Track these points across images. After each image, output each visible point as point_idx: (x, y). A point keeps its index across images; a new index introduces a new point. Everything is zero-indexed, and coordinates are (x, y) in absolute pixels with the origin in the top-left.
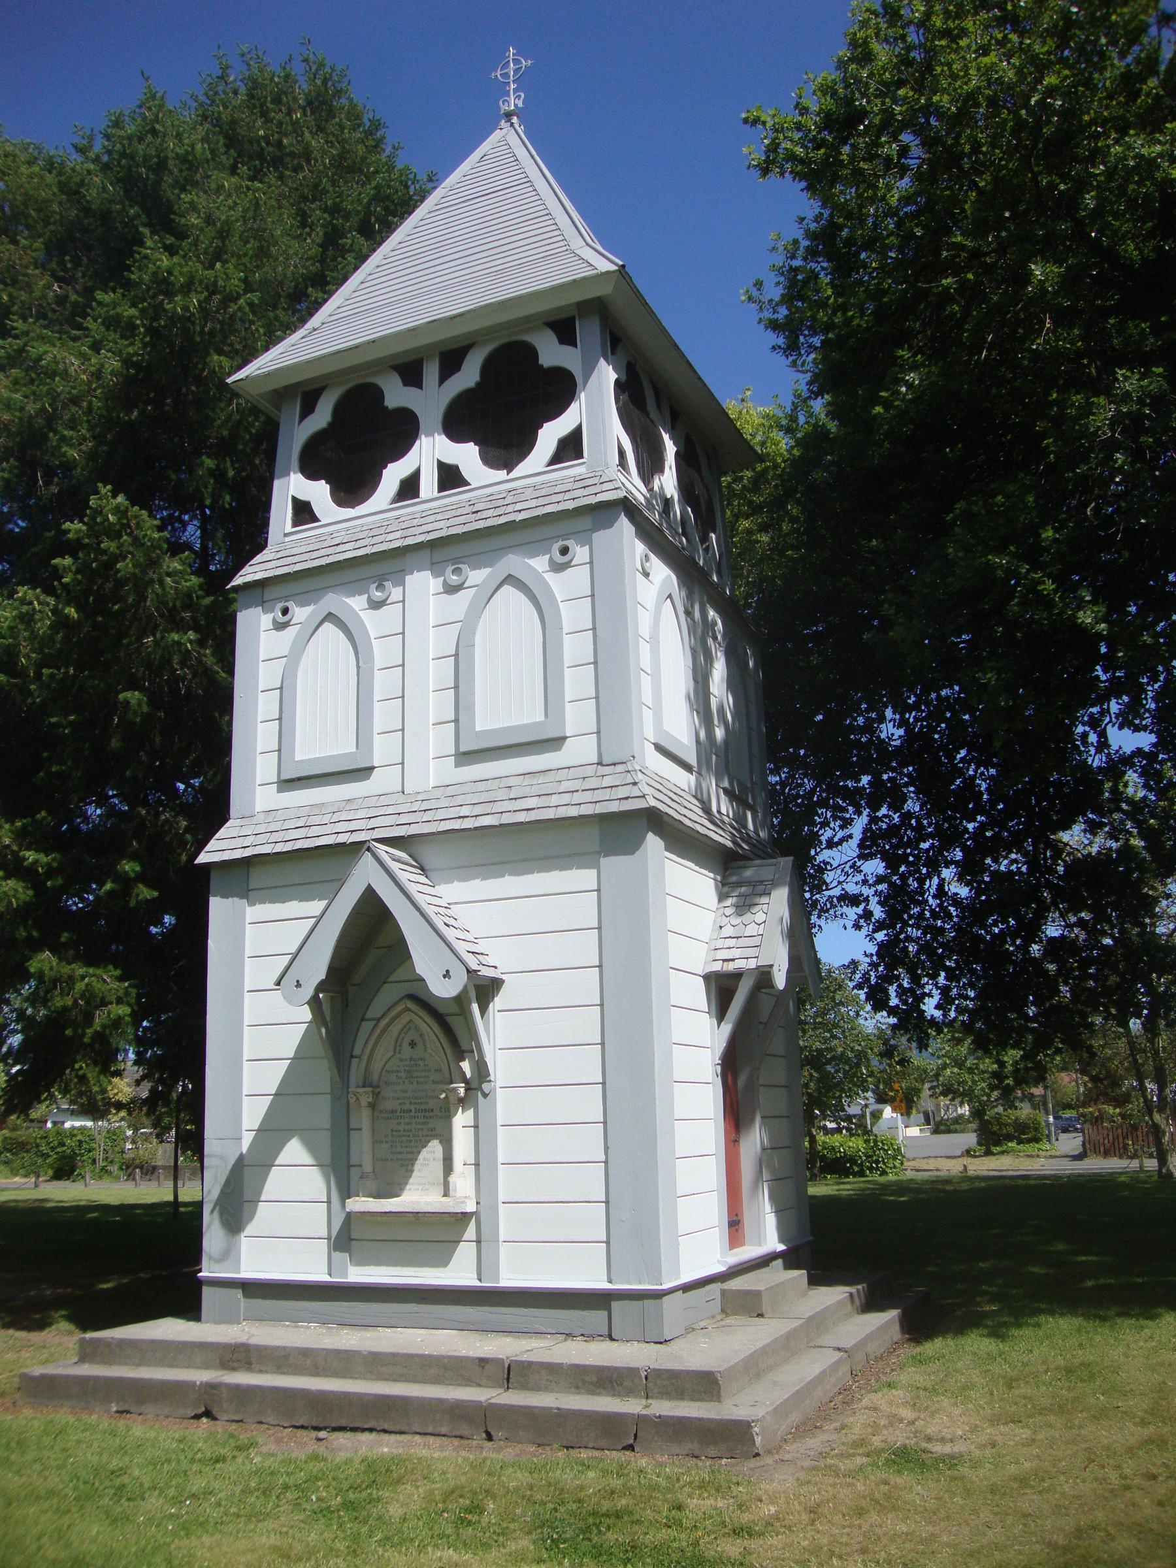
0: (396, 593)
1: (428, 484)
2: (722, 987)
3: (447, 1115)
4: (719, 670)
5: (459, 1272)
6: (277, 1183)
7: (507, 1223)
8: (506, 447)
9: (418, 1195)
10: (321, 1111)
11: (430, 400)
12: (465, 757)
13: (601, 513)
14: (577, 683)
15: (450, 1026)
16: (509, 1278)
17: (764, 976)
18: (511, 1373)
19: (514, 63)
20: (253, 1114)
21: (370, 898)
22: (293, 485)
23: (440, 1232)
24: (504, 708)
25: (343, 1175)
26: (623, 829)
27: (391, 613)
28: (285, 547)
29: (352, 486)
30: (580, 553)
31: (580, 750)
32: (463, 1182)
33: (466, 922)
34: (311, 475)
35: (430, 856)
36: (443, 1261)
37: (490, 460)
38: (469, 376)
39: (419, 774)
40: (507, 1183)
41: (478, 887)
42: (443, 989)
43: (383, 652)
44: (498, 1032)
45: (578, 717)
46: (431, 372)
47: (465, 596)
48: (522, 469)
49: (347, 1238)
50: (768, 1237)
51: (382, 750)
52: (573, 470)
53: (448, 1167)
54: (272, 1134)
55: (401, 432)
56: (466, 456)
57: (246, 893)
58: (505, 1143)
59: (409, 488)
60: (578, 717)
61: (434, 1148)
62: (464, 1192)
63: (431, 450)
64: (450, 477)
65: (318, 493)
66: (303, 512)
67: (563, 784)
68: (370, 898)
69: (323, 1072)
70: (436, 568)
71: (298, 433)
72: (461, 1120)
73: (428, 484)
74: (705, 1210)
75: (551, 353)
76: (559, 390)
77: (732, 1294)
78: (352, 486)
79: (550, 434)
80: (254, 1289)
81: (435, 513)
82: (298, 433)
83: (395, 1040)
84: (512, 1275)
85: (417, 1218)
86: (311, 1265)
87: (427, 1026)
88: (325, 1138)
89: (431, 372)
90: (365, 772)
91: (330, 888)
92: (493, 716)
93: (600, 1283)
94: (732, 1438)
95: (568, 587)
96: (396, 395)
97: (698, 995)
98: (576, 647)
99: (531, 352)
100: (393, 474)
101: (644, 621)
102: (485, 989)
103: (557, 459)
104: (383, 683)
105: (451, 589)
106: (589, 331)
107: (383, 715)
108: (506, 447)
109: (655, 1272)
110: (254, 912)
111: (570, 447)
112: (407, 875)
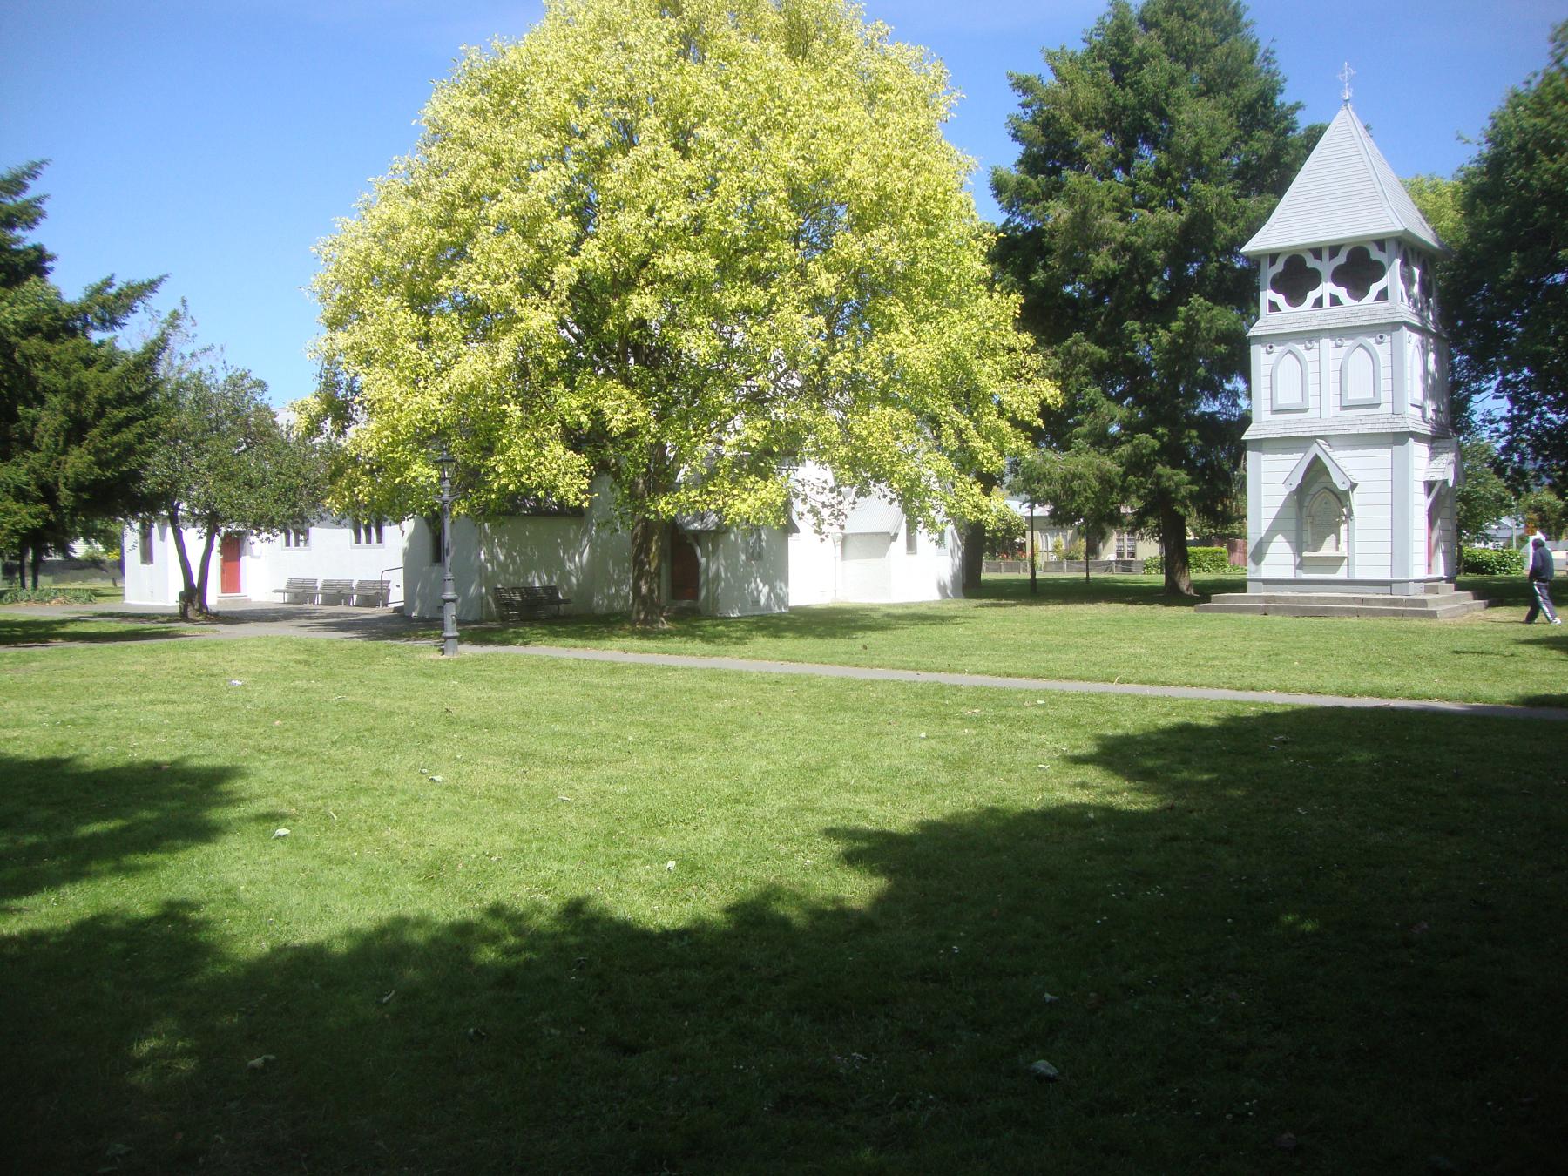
0: (1316, 345)
1: (1326, 301)
2: (1430, 486)
3: (1338, 525)
4: (1432, 356)
5: (1341, 575)
6: (1272, 548)
7: (1357, 560)
8: (1358, 290)
9: (1327, 549)
10: (1292, 524)
11: (1326, 267)
12: (1343, 408)
13: (1396, 326)
14: (1385, 385)
15: (1342, 498)
16: (1358, 577)
17: (1445, 482)
18: (1363, 601)
19: (1348, 71)
20: (1265, 525)
21: (1316, 459)
22: (1268, 295)
23: (1335, 562)
24: (1359, 390)
25: (1298, 548)
26: (1400, 438)
27: (1314, 353)
28: (1265, 324)
29: (1295, 297)
30: (1387, 338)
31: (1386, 408)
32: (1343, 546)
33: (1347, 465)
34: (1277, 291)
35: (1333, 442)
36: (1335, 572)
37: (1352, 296)
38: (1341, 259)
39: (1325, 415)
40: (1358, 547)
41: (1349, 453)
42: (1342, 487)
43: (1311, 368)
44: (1356, 499)
45: (1385, 397)
46: (1326, 255)
47: (1343, 350)
48: (1364, 301)
49: (1299, 566)
50: (1440, 571)
51: (1312, 402)
52: (1383, 304)
53: (1338, 542)
54: (1272, 531)
55: (1314, 279)
56: (1341, 292)
57: (1260, 450)
58: (1358, 535)
59: (1318, 303)
60: (1385, 397)
61: (1333, 536)
62: (1343, 550)
63: (1327, 288)
64: (1335, 301)
65: (1280, 299)
66: (1274, 307)
67: (1380, 421)
68: (1316, 459)
69: (1293, 512)
70: (1332, 337)
71: (1270, 272)
72: (1343, 527)
73: (1326, 301)
74: (1422, 559)
75: (1375, 255)
76: (1378, 271)
77: (1430, 584)
78: (1295, 297)
79: (1375, 288)
80: (1267, 582)
81: (1329, 317)
82: (1270, 272)
83: (1319, 503)
84: (1358, 575)
85: (1327, 558)
86: (1288, 573)
87: (1332, 498)
88: (1293, 538)
89: (1326, 255)
90: (1306, 410)
91: (1305, 450)
92: (1353, 396)
93: (1388, 578)
94: (1433, 615)
95: (1383, 350)
96: (1311, 263)
97: (1421, 488)
98: (1385, 372)
99: (1367, 253)
100: (1312, 296)
101: (1408, 359)
102: (1354, 486)
103: (1377, 299)
104: (1312, 378)
105: (1338, 346)
106: (1390, 247)
107: (1312, 390)
108: (1358, 290)
109: (1406, 574)
110: (1265, 457)
111: (1383, 295)
112: (1328, 450)
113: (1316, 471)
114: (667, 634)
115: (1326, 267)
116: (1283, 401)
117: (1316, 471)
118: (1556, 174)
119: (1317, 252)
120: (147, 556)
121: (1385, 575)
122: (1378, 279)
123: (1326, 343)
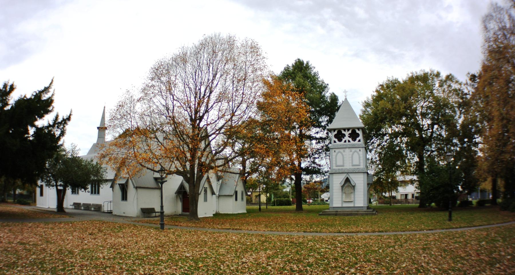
1: (347, 141)
7: (356, 202)
11: (347, 133)
16: (356, 206)
56: (350, 139)
58: (356, 196)
59: (345, 141)
64: (349, 141)
73: (347, 141)
96: (343, 132)
111: (359, 141)
113: (347, 180)
114: (432, 210)
115: (347, 133)
116: (338, 164)
117: (347, 180)
118: (513, 52)
119: (345, 130)
120: (206, 200)
121: (340, 206)
122: (352, 140)
123: (347, 150)
